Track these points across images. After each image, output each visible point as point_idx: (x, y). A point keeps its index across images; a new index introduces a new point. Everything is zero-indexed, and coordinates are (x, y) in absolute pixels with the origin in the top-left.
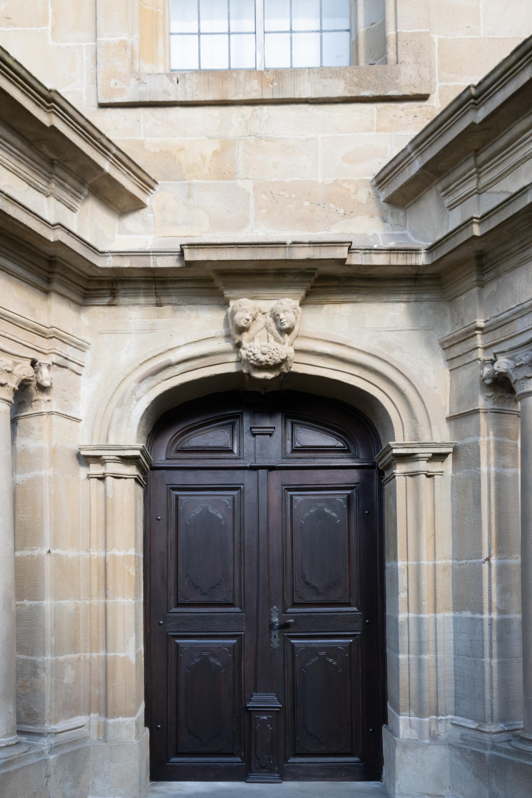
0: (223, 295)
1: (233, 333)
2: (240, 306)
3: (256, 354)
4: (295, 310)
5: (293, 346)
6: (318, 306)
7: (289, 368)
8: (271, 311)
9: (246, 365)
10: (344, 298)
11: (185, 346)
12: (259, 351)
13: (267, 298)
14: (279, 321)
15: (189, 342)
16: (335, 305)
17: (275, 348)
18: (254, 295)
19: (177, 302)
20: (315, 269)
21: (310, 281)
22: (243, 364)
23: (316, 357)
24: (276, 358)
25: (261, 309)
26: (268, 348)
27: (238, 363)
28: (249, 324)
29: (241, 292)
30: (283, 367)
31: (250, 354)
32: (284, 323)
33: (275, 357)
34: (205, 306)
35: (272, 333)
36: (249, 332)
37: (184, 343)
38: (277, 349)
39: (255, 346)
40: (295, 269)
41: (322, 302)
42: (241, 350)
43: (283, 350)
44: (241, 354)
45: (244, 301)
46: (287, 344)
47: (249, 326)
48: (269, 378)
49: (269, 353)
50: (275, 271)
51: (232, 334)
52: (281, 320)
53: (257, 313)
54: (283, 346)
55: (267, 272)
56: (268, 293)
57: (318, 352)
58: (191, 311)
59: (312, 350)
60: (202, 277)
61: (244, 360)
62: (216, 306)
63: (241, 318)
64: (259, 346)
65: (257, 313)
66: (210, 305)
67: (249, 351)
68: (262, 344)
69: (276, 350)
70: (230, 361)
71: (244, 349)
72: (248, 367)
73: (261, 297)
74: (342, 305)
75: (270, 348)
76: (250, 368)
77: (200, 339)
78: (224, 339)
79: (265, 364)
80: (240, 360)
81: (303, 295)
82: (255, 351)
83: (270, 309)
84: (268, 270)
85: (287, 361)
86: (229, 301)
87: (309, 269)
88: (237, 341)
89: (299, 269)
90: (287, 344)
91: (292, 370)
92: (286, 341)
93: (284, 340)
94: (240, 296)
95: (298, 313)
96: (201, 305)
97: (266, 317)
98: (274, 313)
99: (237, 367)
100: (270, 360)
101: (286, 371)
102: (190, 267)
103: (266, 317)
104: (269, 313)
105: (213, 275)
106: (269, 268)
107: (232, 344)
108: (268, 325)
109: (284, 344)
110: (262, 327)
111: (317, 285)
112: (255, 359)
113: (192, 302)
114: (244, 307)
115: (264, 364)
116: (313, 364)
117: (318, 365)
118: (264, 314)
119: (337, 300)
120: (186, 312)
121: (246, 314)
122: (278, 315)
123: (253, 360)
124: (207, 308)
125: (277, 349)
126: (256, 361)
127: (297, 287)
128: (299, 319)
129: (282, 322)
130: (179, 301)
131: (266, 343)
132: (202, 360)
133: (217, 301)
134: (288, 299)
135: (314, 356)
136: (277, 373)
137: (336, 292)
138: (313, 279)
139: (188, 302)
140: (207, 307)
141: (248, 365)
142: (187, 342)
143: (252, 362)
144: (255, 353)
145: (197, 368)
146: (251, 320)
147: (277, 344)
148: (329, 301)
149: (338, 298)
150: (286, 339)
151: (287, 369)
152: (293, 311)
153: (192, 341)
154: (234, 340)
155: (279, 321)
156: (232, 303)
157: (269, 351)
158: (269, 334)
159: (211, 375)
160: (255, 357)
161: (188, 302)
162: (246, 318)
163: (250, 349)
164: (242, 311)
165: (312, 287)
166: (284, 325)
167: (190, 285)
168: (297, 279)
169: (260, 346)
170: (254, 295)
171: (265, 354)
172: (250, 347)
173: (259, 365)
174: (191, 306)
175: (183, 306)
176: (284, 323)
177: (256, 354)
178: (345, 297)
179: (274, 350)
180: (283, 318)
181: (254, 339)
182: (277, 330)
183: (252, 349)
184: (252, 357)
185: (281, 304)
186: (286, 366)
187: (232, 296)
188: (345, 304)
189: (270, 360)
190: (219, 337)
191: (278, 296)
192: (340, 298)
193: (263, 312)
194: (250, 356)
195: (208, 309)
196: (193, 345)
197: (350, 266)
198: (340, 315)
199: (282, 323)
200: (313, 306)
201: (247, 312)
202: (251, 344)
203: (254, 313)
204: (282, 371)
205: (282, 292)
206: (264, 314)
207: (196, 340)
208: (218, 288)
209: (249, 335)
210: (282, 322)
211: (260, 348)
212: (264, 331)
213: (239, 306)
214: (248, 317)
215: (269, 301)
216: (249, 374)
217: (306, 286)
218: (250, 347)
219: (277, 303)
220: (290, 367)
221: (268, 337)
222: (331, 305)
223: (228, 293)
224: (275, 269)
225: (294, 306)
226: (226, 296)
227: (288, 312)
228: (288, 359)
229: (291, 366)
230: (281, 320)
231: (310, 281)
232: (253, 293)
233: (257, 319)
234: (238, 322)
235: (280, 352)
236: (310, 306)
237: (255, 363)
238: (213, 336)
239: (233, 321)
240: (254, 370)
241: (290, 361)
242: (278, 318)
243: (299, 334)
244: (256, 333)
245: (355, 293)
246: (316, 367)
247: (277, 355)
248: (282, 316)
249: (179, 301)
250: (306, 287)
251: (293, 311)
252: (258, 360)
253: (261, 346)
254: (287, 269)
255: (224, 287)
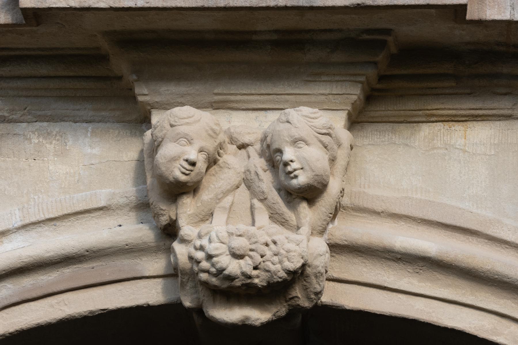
0: (134, 98)
1: (154, 198)
2: (172, 126)
3: (216, 256)
4: (326, 139)
5: (326, 236)
6: (402, 126)
7: (313, 296)
8: (264, 139)
9: (190, 284)
10: (474, 107)
11: (23, 231)
12: (224, 248)
13: (255, 107)
14: (281, 166)
15: (33, 219)
16: (451, 124)
17: (269, 240)
18: (217, 98)
19: (6, 114)
20: (388, 32)
21: (375, 63)
22: (182, 282)
23: (395, 265)
24: (272, 268)
25: (235, 135)
26: (249, 239)
27: (170, 280)
28: (198, 174)
29: (183, 88)
30: (297, 292)
31: (200, 255)
32: (296, 173)
33: (269, 263)
34: (85, 125)
35: (263, 200)
36: (198, 195)
37: (19, 224)
38: (275, 243)
39: (213, 235)
40: (330, 31)
41: (413, 116)
42: (177, 247)
43: (291, 246)
44: (175, 256)
45: (186, 111)
46: (305, 230)
47: (195, 180)
48: (257, 323)
49: (251, 253)
50: (275, 37)
51: (151, 201)
52: (286, 164)
53: (221, 146)
54: (293, 236)
55: (255, 37)
56: (249, 92)
57: (398, 253)
58: (45, 138)
59: (381, 245)
60: (78, 49)
61: (184, 273)
62: (118, 125)
63: (174, 159)
64: (224, 234)
65: (221, 146)
66: (99, 122)
67: (196, 249)
68: (232, 228)
69: (272, 246)
70: (147, 275)
71: (183, 241)
72: (196, 292)
73: (237, 102)
74: (470, 124)
75: (254, 240)
76: (203, 295)
77: (66, 212)
78: (133, 214)
79: (243, 285)
80: (172, 272)
81: (355, 98)
82: (211, 248)
83: (260, 136)
84: (255, 32)
85: (308, 276)
86: (150, 113)
87: (368, 31)
88: (164, 220)
89: (340, 31)
90: (305, 230)
91: (325, 299)
92: (303, 221)
93: (298, 218)
94: (179, 100)
95: (339, 145)
96: (76, 122)
97: (249, 157)
98: (268, 146)
99: (166, 290)
100: (255, 273)
101: (306, 304)
102: (38, 25)
103: (249, 157)
104: (258, 146)
105: (105, 45)
106: (258, 29)
107: (150, 228)
108: (253, 176)
109: (298, 228)
110: (236, 183)
111: (396, 72)
112: (213, 270)
113: (49, 113)
114: (183, 129)
115: (238, 283)
116: (386, 285)
117: (402, 288)
118: (242, 147)
119: (454, 112)
120: (30, 139)
121: (188, 148)
122: (280, 151)
123: (207, 271)
124: (90, 129)
125: (275, 243)
126: (215, 275)
127: (337, 78)
128: (341, 162)
129: (289, 169)
130: (12, 111)
131: (243, 227)
132: (67, 271)
133: (118, 113)
134: (306, 110)
135: (390, 263)
136: (282, 310)
137: (451, 91)
138: (380, 57)
139: (39, 113)
140: (90, 127)
141: (195, 287)
142: (27, 221)
143: (204, 276)
144: (213, 253)
145: (50, 291)
146: (201, 165)
147: (275, 228)
148: (433, 115)
149: (458, 106)
150: (302, 215)
151: (309, 298)
152: (321, 142)
153: (42, 217)
154: (156, 216)
155: (281, 166)
156: (156, 118)
157: (253, 247)
158: (256, 202)
159: (91, 312)
160: (213, 265)
161: (39, 113)
162: (186, 157)
163: (198, 243)
164: (176, 139)
165: (381, 78)
166: (296, 177)
167: (44, 70)
168: (337, 57)
169: (225, 234)
170: (217, 98)
171: (240, 257)
172: (200, 237)
173: (225, 285)
174: (45, 124)
175: (24, 125)
176: (296, 173)
177: (216, 256)
178: (479, 105)
179: (267, 245)
180: (293, 158)
181: (212, 214)
182: (279, 190)
183: (205, 242)
184: (205, 265)
185: (288, 122)
186: (305, 289)
187: (157, 99)
188: (480, 123)
189: (255, 273)
190: (120, 207)
191: (287, 101)
192: (463, 106)
193: (239, 143)
194: (198, 262)
195: (93, 132)
196: (45, 230)
197: (480, 23)
198: (465, 151)
199: (290, 173)
200: (388, 126)
201: (190, 142)
202: (204, 227)
203: (210, 145)
204: (292, 302)
205: (297, 91)
206: (242, 147)
207: (52, 216)
208: (120, 78)
209: (199, 204)
210: (289, 169)
211: (226, 240)
212: (243, 192)
213: (168, 127)
214: (193, 155)
215: (263, 113)
216: (199, 311)
217: (363, 75)
218: (200, 237)
219: (278, 120)
220: (318, 294)
221: (252, 208)
222: (439, 126)
223: (146, 92)
224: (276, 31)
225: (324, 128)
226: (140, 99)
227: (307, 143)
228: (309, 270)
229: (318, 289)
230: (286, 164)
231: (375, 63)
232: (216, 91)
233: (221, 161)
234: (163, 169)
235: (282, 252)
236: (380, 126)
237: (214, 281)
238: (102, 204)
239: (154, 167)
240: (214, 301)
241: (316, 277)
242: (278, 158)
243: (346, 201)
244: (218, 200)
245: (505, 94)
246: (395, 294)
247: (276, 259)
248: (289, 154)
249: (12, 111)
250: (363, 79)
251: (321, 142)
252: (221, 271)
253: (231, 234)
254: (309, 31)
255: (135, 77)
